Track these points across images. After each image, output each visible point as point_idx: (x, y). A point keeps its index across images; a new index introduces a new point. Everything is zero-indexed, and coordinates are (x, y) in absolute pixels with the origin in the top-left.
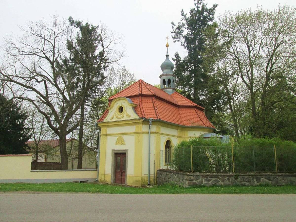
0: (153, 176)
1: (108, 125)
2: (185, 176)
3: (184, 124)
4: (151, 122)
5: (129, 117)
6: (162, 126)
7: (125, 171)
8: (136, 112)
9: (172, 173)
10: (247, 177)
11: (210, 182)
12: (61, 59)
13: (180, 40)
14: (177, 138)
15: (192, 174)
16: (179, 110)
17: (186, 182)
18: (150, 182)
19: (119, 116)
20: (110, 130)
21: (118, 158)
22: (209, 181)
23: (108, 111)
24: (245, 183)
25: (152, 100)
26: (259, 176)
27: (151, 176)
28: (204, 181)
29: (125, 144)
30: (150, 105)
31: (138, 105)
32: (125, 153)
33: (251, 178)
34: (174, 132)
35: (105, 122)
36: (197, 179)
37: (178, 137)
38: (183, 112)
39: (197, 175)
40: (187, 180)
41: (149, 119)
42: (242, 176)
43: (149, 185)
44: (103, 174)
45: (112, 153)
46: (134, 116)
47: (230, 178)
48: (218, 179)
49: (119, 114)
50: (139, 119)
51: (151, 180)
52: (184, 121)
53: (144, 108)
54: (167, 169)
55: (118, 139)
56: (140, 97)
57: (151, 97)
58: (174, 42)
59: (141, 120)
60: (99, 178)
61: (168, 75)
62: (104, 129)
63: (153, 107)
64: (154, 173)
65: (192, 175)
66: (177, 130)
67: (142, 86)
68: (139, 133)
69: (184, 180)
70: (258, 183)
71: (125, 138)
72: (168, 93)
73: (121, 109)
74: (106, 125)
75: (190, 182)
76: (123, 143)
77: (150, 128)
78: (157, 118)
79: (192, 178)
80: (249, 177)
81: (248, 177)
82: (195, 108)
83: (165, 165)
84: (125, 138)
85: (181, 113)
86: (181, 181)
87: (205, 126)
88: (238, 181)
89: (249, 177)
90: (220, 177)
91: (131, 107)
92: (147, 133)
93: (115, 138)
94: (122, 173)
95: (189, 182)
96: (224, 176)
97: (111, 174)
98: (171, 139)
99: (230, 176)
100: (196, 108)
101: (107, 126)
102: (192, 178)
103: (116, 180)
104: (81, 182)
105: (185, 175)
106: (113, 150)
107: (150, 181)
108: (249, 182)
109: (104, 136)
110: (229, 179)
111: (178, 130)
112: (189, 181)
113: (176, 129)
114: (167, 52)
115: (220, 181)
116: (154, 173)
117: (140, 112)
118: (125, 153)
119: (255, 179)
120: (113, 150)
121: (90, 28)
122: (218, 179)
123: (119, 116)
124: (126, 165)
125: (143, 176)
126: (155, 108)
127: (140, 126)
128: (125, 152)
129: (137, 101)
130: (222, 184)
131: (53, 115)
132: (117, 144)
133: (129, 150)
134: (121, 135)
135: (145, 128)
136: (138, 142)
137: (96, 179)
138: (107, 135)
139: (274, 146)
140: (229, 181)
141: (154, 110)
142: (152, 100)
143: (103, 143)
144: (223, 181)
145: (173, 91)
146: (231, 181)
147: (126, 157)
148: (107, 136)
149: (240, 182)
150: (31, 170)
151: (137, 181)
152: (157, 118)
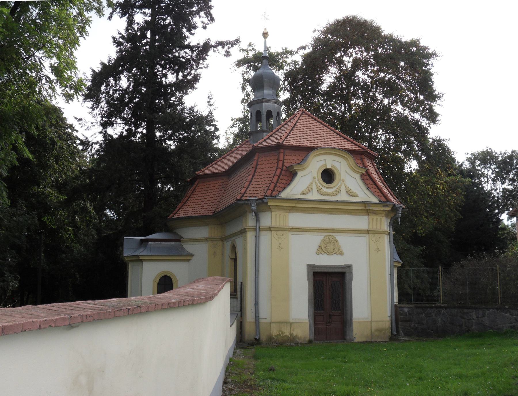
19: (325, 190)
29: (317, 253)
45: (308, 272)
55: (324, 241)
58: (444, 100)
68: (382, 232)
71: (342, 240)
84: (342, 240)
91: (358, 176)
93: (317, 239)
101: (292, 209)
106: (310, 266)
114: (265, 41)
120: (310, 266)
121: (70, 101)
123: (325, 190)
127: (379, 218)
131: (123, 114)
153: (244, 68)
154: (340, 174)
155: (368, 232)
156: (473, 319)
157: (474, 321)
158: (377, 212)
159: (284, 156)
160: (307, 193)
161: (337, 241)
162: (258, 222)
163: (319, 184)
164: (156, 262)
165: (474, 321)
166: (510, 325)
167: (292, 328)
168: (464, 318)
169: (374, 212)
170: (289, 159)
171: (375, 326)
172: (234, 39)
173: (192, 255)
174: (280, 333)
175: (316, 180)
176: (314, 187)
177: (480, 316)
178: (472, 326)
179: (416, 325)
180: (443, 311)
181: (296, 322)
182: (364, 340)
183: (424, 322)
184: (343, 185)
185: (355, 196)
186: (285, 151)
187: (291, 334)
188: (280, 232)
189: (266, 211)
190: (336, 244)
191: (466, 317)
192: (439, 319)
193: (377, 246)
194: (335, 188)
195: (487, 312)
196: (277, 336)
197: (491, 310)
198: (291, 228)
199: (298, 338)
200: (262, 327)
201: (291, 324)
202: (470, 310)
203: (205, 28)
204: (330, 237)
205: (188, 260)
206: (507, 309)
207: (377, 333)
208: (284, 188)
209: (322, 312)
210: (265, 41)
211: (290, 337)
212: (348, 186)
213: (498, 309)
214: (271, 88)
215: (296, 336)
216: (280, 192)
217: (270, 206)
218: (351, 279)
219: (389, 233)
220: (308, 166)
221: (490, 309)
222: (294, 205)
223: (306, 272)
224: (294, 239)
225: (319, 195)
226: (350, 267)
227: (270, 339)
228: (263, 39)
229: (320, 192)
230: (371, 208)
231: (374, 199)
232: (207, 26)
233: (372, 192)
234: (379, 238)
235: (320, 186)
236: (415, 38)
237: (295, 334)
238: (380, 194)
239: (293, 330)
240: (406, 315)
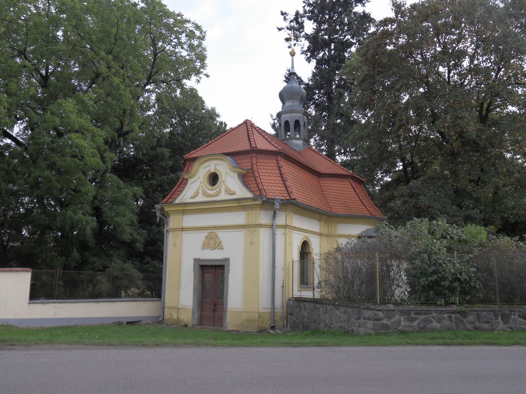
0: (280, 310)
1: (186, 208)
2: (364, 311)
3: (332, 209)
4: (277, 205)
5: (232, 194)
6: (296, 213)
7: (223, 302)
8: (246, 185)
9: (329, 305)
10: (485, 313)
11: (415, 323)
13: (299, 43)
14: (318, 237)
15: (380, 308)
16: (321, 182)
17: (366, 323)
18: (274, 323)
19: (209, 192)
20: (189, 221)
21: (206, 275)
22: (413, 320)
23: (184, 182)
24: (482, 324)
25: (277, 161)
26: (508, 312)
27: (276, 310)
28: (403, 321)
29: (222, 249)
30: (273, 171)
31: (251, 171)
33: (493, 315)
34: (313, 225)
35: (177, 204)
36: (389, 318)
37: (320, 236)
38: (329, 185)
39: (390, 310)
40: (369, 319)
41: (274, 199)
42: (475, 311)
43: (273, 328)
44: (175, 308)
45: (194, 265)
46: (242, 192)
47: (453, 316)
48: (431, 316)
49: (209, 187)
50: (254, 199)
51: (277, 318)
52: (331, 204)
53: (261, 177)
54: (314, 298)
55: (207, 237)
56: (254, 155)
57: (274, 155)
59: (258, 200)
60: (167, 315)
61: (294, 113)
62: (176, 218)
63: (279, 175)
64: (283, 304)
65: (380, 310)
66: (318, 222)
67: (252, 132)
69: (362, 319)
70: (505, 324)
71: (222, 235)
72: (295, 148)
73: (214, 179)
74: (182, 208)
75: (376, 322)
76: (218, 245)
77: (274, 217)
78: (290, 196)
79: (381, 314)
80: (489, 313)
81: (486, 313)
82: (350, 179)
83: (300, 289)
84: (222, 235)
85: (325, 188)
86: (353, 320)
87: (371, 214)
88: (467, 321)
89: (488, 314)
90: (433, 313)
91: (235, 175)
92: (270, 226)
93: (201, 236)
94: (215, 305)
95: (374, 324)
96: (442, 311)
97: (191, 308)
98: (310, 238)
99: (453, 312)
100: (352, 179)
101: (184, 212)
102: (381, 314)
103: (202, 320)
104: (128, 323)
105: (364, 309)
107: (274, 321)
108: (489, 322)
109: (176, 232)
110: (450, 317)
111: (320, 220)
112: (375, 322)
113: (316, 219)
114: (293, 59)
115: (433, 322)
116: (283, 304)
117: (256, 185)
118: (223, 266)
119: (499, 317)
120: (196, 260)
122: (431, 316)
123: (209, 192)
125: (261, 310)
126: (284, 179)
128: (222, 264)
129: (246, 163)
130: (438, 326)
132: (205, 246)
133: (197, 257)
136: (252, 243)
137: (160, 317)
138: (183, 229)
140: (451, 321)
141: (282, 182)
142: (277, 161)
143: (175, 245)
144: (439, 321)
145: (304, 145)
146: (454, 321)
147: (224, 273)
148: (182, 231)
149: (472, 323)
151: (249, 321)
152: (290, 196)
155: (242, 227)
161: (217, 237)
163: (205, 188)
167: (179, 313)
181: (184, 308)
185: (233, 194)
193: (252, 240)
194: (217, 190)
201: (178, 309)
204: (212, 234)
206: (337, 305)
210: (293, 59)
212: (228, 185)
225: (204, 197)
226: (227, 260)
228: (290, 57)
229: (205, 194)
237: (181, 318)
239: (180, 315)
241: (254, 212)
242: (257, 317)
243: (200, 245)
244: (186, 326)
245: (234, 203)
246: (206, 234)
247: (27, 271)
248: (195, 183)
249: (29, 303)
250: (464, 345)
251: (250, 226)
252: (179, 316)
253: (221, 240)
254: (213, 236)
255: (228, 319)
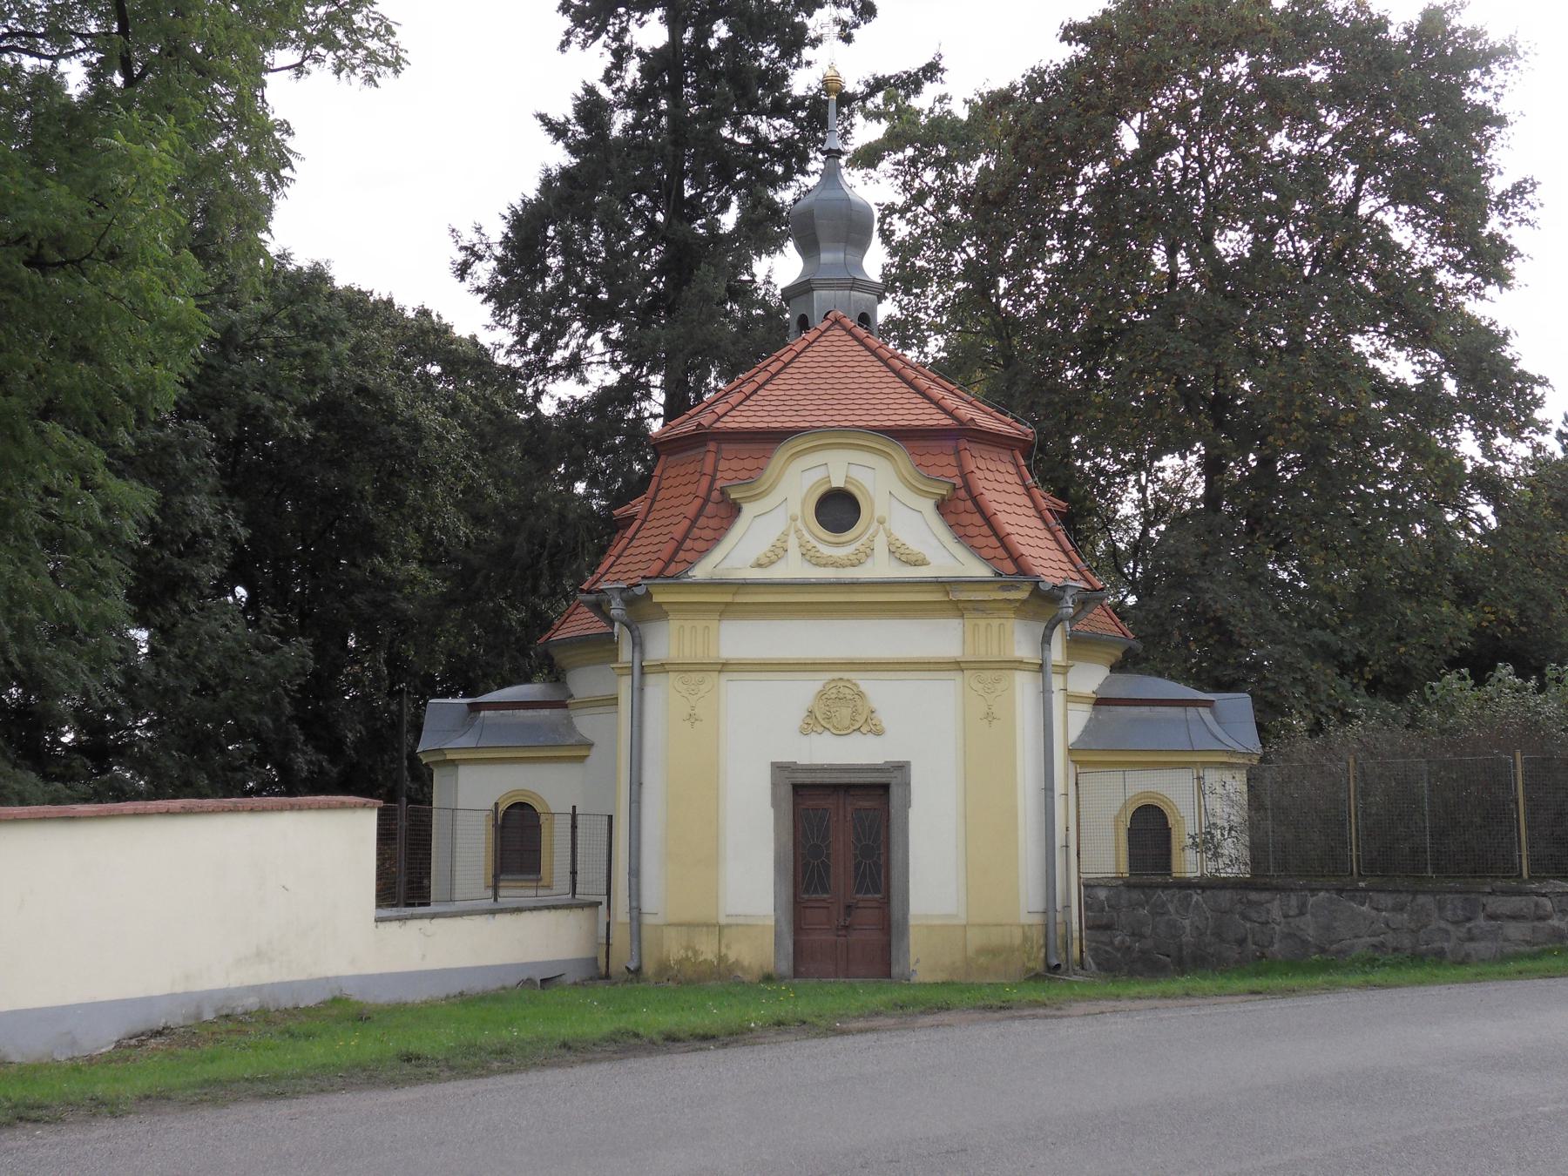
5: (915, 564)
12: (122, 57)
19: (826, 551)
29: (804, 732)
32: (885, 788)
55: (821, 694)
58: (1541, 205)
59: (1017, 588)
65: (1544, 895)
71: (875, 689)
84: (875, 689)
91: (928, 506)
93: (807, 689)
97: (772, 923)
101: (727, 611)
106: (778, 768)
112: (1536, 923)
120: (778, 768)
123: (826, 551)
124: (896, 855)
125: (1026, 919)
128: (884, 780)
132: (813, 722)
134: (846, 675)
135: (1019, 639)
136: (990, 717)
138: (724, 667)
139: (1514, 758)
142: (958, 452)
150: (378, 906)
151: (992, 952)
153: (464, 253)
154: (872, 504)
155: (957, 666)
156: (1274, 921)
157: (1277, 928)
158: (987, 606)
159: (716, 461)
160: (772, 563)
161: (860, 694)
162: (637, 649)
163: (807, 536)
164: (554, 765)
165: (1277, 928)
166: (1374, 940)
167: (724, 942)
168: (1251, 920)
169: (979, 608)
170: (729, 467)
171: (976, 939)
172: (922, 64)
173: (590, 745)
174: (690, 954)
175: (799, 524)
176: (793, 543)
177: (1291, 913)
178: (1271, 943)
179: (1128, 939)
180: (1195, 897)
181: (737, 925)
182: (941, 977)
183: (1147, 931)
184: (882, 532)
185: (920, 562)
186: (723, 446)
187: (722, 958)
188: (693, 675)
189: (659, 619)
190: (859, 703)
191: (1254, 915)
192: (1187, 923)
194: (857, 545)
195: (1311, 900)
196: (680, 962)
197: (1322, 894)
198: (723, 664)
199: (743, 968)
200: (647, 934)
201: (721, 928)
202: (1265, 896)
203: (848, 39)
204: (840, 684)
205: (582, 759)
206: (1363, 889)
207: (982, 960)
208: (704, 553)
209: (825, 896)
211: (719, 964)
213: (1340, 891)
214: (842, 244)
215: (737, 962)
216: (692, 564)
217: (659, 604)
218: (907, 804)
219: (1041, 665)
220: (772, 487)
221: (1320, 890)
222: (728, 598)
223: (769, 785)
224: (737, 694)
225: (895, 563)
226: (902, 768)
227: (664, 969)
229: (809, 556)
230: (964, 596)
231: (978, 569)
232: (853, 31)
233: (975, 550)
234: (998, 681)
235: (811, 539)
236: (320, 257)
237: (732, 957)
238: (1001, 553)
239: (728, 947)
240: (1102, 910)
241: (995, 623)
242: (1018, 941)
243: (798, 716)
244: (768, 978)
245: (931, 592)
246: (818, 686)
247: (364, 806)
248: (764, 517)
249: (379, 920)
250: (58, 1120)
251: (986, 665)
252: (724, 950)
253: (874, 705)
254: (847, 691)
255: (913, 950)
